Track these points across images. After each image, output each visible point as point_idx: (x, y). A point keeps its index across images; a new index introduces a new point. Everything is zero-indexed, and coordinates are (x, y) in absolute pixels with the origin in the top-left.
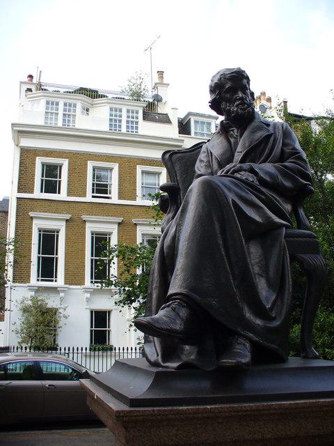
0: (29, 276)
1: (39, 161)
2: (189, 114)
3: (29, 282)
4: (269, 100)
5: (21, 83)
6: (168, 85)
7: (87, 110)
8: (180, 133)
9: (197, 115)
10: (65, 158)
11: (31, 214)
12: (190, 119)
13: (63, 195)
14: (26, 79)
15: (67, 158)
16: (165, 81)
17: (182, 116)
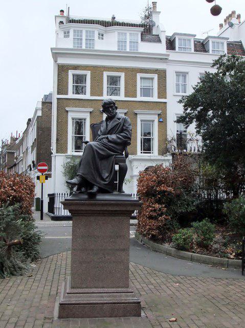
0: (67, 149)
1: (71, 73)
2: (175, 34)
3: (67, 153)
4: (239, 17)
5: (56, 17)
6: (160, 12)
7: (102, 35)
8: (167, 48)
9: (178, 34)
10: (88, 70)
11: (67, 109)
12: (175, 39)
13: (88, 96)
14: (59, 13)
15: (90, 70)
16: (158, 10)
17: (171, 35)
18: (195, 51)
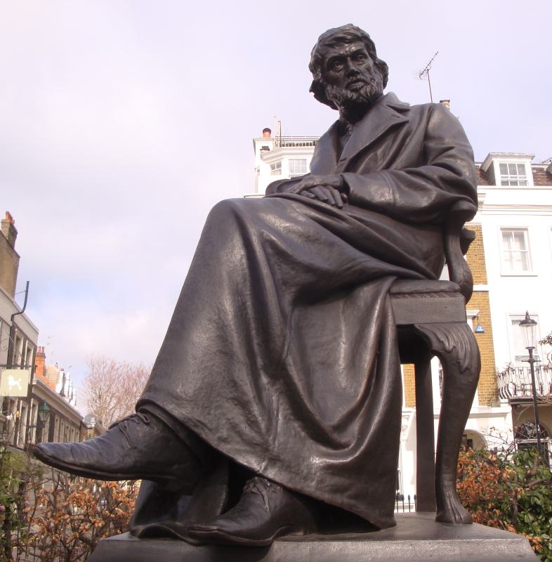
18: (536, 184)
